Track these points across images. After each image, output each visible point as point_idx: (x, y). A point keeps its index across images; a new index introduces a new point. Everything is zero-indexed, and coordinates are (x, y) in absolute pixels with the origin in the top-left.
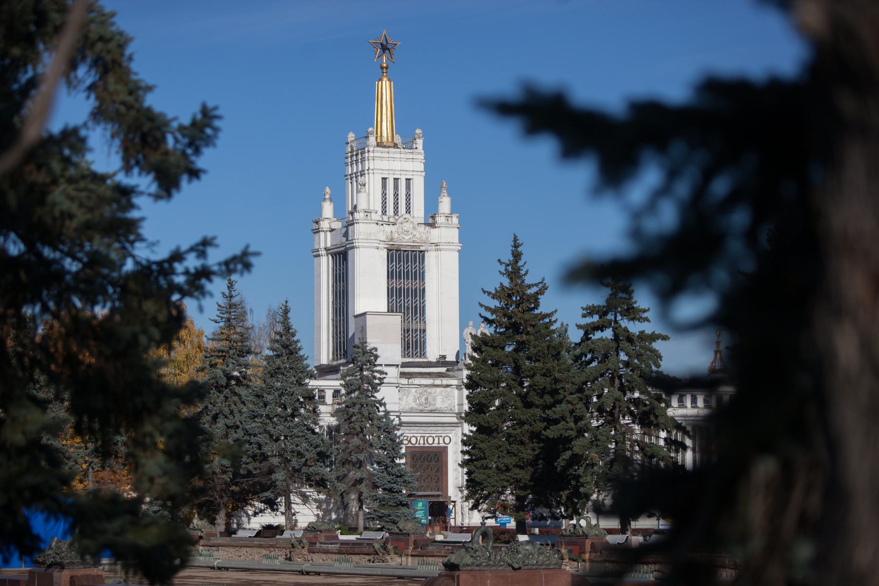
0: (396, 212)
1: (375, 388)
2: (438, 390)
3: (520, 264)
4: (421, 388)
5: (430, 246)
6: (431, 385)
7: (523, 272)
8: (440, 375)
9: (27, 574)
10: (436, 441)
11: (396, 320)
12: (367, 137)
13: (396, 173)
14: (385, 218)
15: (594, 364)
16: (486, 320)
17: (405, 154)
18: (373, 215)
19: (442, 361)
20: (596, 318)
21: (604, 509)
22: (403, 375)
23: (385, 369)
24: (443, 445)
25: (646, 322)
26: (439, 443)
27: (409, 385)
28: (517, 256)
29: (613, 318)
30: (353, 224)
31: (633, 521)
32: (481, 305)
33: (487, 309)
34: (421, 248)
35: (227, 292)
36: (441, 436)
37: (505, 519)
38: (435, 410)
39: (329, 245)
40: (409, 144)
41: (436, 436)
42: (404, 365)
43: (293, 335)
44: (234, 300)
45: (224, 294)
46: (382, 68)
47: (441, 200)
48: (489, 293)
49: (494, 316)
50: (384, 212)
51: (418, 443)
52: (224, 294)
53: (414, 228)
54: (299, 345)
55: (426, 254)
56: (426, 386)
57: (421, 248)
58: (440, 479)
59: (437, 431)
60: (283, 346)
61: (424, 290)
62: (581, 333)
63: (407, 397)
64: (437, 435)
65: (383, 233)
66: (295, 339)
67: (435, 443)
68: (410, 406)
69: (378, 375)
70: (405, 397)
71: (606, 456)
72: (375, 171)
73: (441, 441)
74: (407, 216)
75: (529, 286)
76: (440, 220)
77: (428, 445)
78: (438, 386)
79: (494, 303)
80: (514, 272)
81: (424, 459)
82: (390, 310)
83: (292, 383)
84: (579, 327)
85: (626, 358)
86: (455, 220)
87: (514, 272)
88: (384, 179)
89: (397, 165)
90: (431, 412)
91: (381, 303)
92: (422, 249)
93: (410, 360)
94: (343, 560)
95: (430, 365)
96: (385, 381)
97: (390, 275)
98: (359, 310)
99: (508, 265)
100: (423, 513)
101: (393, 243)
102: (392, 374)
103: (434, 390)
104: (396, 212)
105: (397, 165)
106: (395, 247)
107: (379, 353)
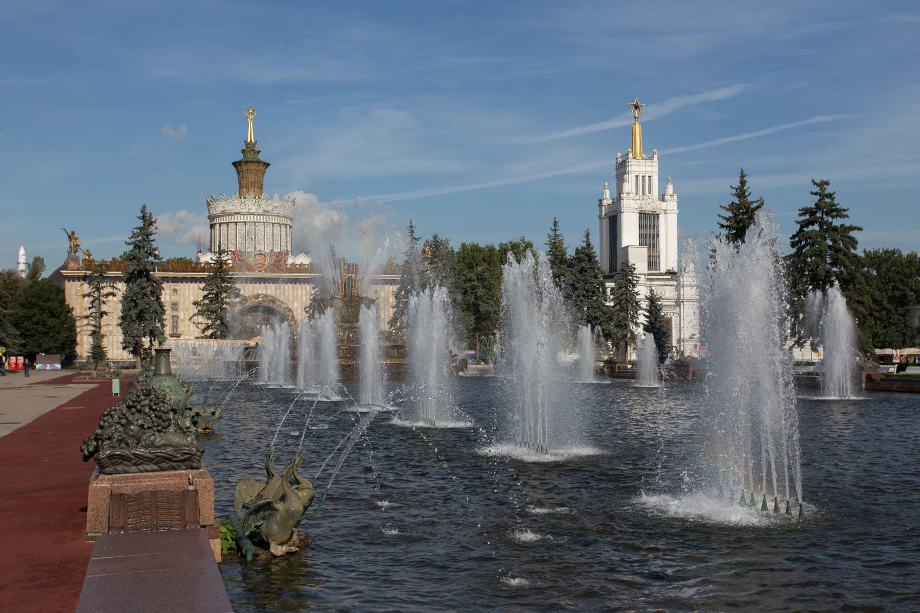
1: (634, 286)
2: (667, 287)
3: (745, 188)
7: (747, 194)
8: (668, 280)
11: (644, 250)
12: (628, 154)
14: (638, 197)
15: (808, 248)
16: (722, 226)
17: (648, 163)
19: (669, 273)
20: (807, 217)
22: (648, 279)
23: (640, 276)
24: (669, 317)
25: (847, 218)
28: (743, 183)
29: (820, 215)
32: (719, 216)
33: (724, 218)
35: (553, 228)
42: (649, 275)
43: (592, 249)
44: (558, 233)
45: (551, 229)
46: (635, 118)
48: (725, 208)
49: (728, 223)
50: (637, 194)
52: (551, 229)
54: (596, 254)
55: (660, 216)
56: (661, 285)
60: (586, 255)
62: (798, 226)
66: (593, 251)
69: (635, 279)
74: (649, 195)
75: (752, 203)
76: (667, 197)
78: (666, 285)
79: (729, 214)
80: (741, 193)
82: (641, 244)
83: (591, 276)
84: (798, 222)
85: (830, 243)
86: (675, 197)
87: (741, 193)
88: (637, 176)
89: (642, 169)
91: (636, 241)
92: (657, 213)
93: (651, 272)
94: (879, 436)
95: (661, 274)
96: (639, 282)
97: (641, 227)
98: (624, 244)
99: (737, 189)
102: (642, 279)
103: (664, 287)
104: (643, 194)
106: (644, 212)
107: (636, 267)
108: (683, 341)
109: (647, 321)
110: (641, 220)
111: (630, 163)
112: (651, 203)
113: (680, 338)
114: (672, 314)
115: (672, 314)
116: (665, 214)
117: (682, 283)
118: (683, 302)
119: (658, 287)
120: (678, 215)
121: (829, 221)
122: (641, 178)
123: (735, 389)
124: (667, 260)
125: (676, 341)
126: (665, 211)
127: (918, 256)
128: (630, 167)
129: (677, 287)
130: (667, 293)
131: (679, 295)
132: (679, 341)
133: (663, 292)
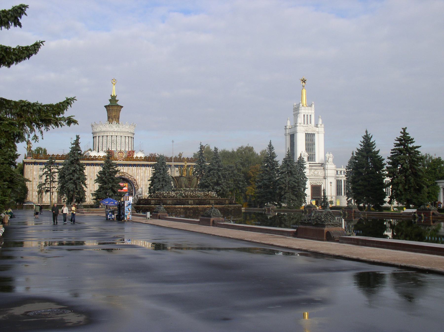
9: (394, 220)
18: (302, 124)
24: (320, 184)
30: (296, 126)
31: (126, 190)
39: (289, 132)
40: (311, 106)
46: (303, 86)
50: (304, 124)
53: (312, 128)
72: (302, 108)
76: (319, 126)
86: (323, 126)
88: (304, 115)
89: (307, 111)
97: (306, 140)
104: (307, 124)
105: (307, 111)
114: (322, 183)
115: (322, 183)
126: (318, 132)
131: (325, 174)
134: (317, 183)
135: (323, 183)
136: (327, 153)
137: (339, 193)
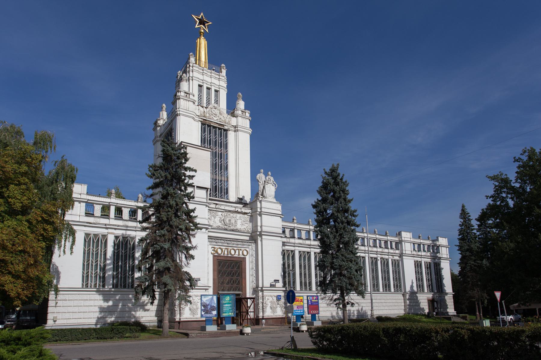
0: (208, 102)
4: (226, 213)
5: (231, 127)
6: (234, 211)
10: (237, 253)
13: (208, 83)
21: (7, 275)
26: (239, 255)
27: (216, 209)
34: (225, 127)
36: (241, 250)
37: (300, 311)
38: (236, 230)
41: (237, 250)
47: (238, 102)
51: (223, 253)
56: (230, 211)
57: (225, 127)
58: (240, 282)
59: (238, 245)
61: (227, 189)
63: (215, 218)
64: (238, 248)
65: (198, 111)
67: (236, 254)
68: (217, 225)
70: (213, 218)
71: (334, 264)
73: (241, 253)
74: (216, 105)
77: (230, 255)
81: (233, 282)
86: (248, 115)
88: (200, 86)
89: (208, 79)
90: (233, 230)
92: (226, 127)
100: (230, 306)
101: (205, 119)
103: (235, 215)
108: (262, 291)
109: (412, 287)
110: (205, 132)
111: (191, 68)
112: (218, 114)
113: (257, 286)
114: (245, 253)
115: (245, 253)
116: (235, 131)
117: (259, 210)
118: (261, 235)
119: (225, 214)
120: (252, 137)
121: (324, 204)
122: (205, 90)
123: (315, 333)
124: (237, 188)
125: (252, 291)
126: (235, 127)
127: (537, 151)
128: (191, 73)
129: (251, 216)
130: (239, 222)
131: (255, 226)
132: (255, 290)
133: (233, 221)
134: (233, 252)
135: (250, 253)
136: (260, 173)
137: (305, 285)
